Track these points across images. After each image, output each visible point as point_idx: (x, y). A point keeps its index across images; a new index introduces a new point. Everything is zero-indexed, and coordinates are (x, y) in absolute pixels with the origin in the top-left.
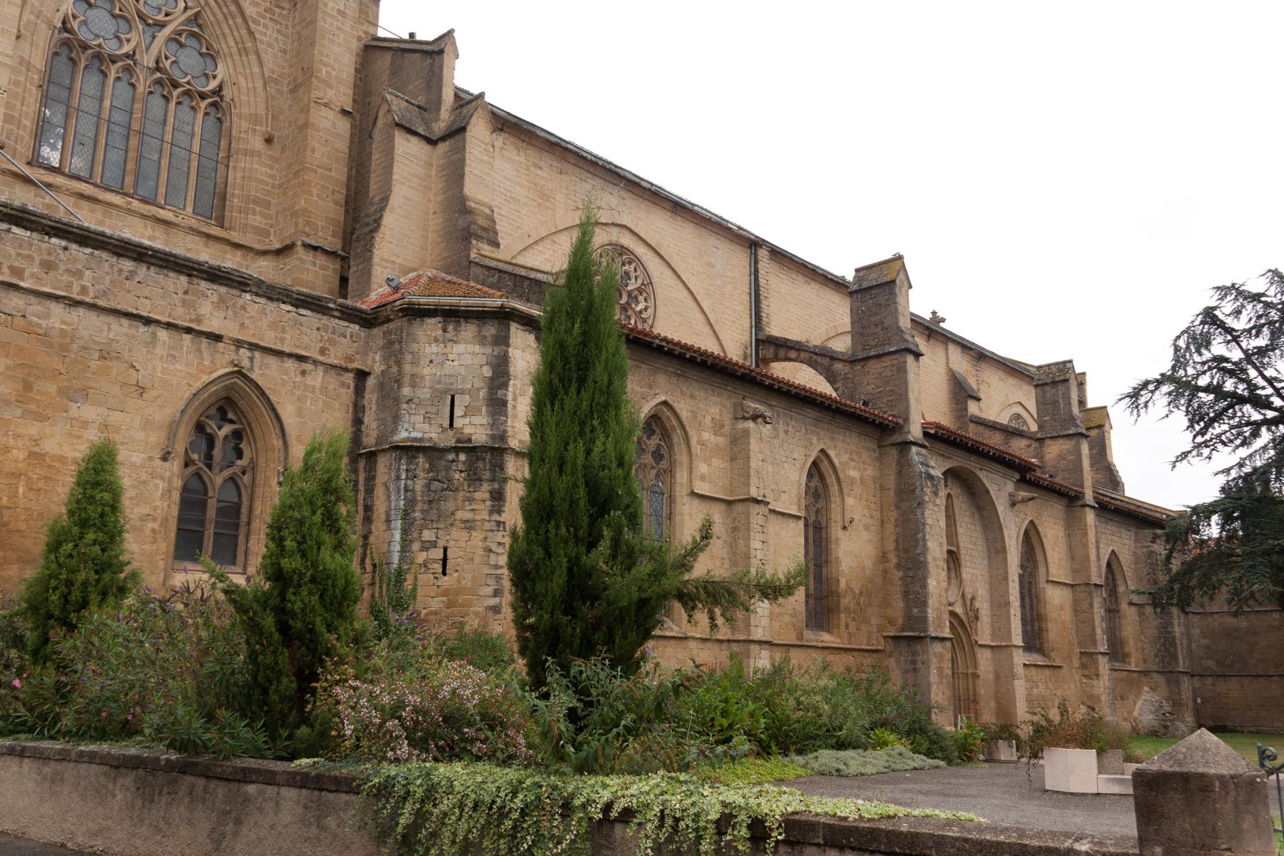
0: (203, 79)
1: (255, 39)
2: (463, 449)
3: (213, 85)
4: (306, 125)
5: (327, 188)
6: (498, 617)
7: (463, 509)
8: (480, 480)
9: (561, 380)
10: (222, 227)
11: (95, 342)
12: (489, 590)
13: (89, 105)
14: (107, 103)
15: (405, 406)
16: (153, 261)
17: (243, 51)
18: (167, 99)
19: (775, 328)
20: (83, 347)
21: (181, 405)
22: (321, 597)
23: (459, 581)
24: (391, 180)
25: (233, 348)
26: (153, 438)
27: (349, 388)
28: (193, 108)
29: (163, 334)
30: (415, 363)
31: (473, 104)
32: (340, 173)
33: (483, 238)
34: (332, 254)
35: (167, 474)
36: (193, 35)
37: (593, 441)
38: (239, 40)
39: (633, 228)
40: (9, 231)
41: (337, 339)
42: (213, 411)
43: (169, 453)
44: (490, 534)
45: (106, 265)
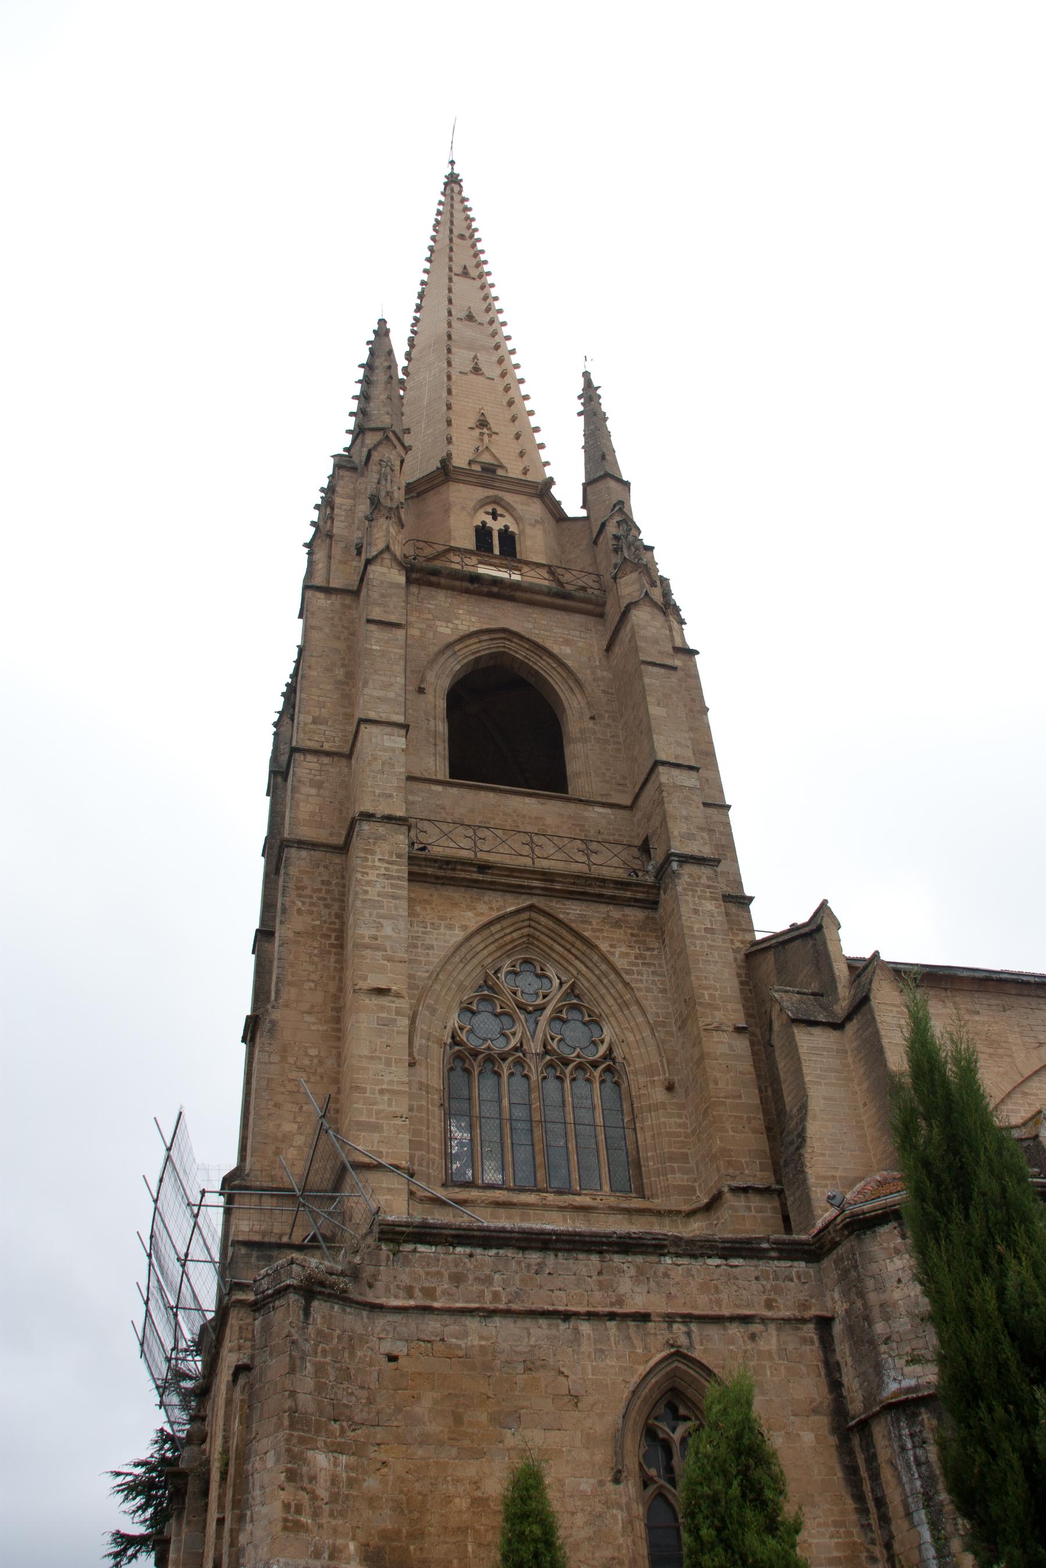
0: (592, 1047)
1: (632, 989)
3: (602, 1049)
4: (702, 1057)
5: (741, 1118)
9: (939, 1206)
10: (644, 1197)
13: (490, 1110)
14: (505, 1102)
15: (883, 1348)
16: (559, 1246)
18: (560, 1079)
20: (506, 1362)
21: (621, 1408)
24: (804, 1083)
25: (665, 1325)
26: (599, 1458)
28: (588, 1080)
29: (585, 1327)
30: (880, 1288)
31: (870, 968)
32: (751, 1097)
34: (764, 1191)
35: (624, 1500)
36: (574, 1007)
37: (1003, 1274)
40: (415, 1251)
41: (783, 1285)
42: (661, 1410)
43: (619, 1472)
45: (514, 1263)
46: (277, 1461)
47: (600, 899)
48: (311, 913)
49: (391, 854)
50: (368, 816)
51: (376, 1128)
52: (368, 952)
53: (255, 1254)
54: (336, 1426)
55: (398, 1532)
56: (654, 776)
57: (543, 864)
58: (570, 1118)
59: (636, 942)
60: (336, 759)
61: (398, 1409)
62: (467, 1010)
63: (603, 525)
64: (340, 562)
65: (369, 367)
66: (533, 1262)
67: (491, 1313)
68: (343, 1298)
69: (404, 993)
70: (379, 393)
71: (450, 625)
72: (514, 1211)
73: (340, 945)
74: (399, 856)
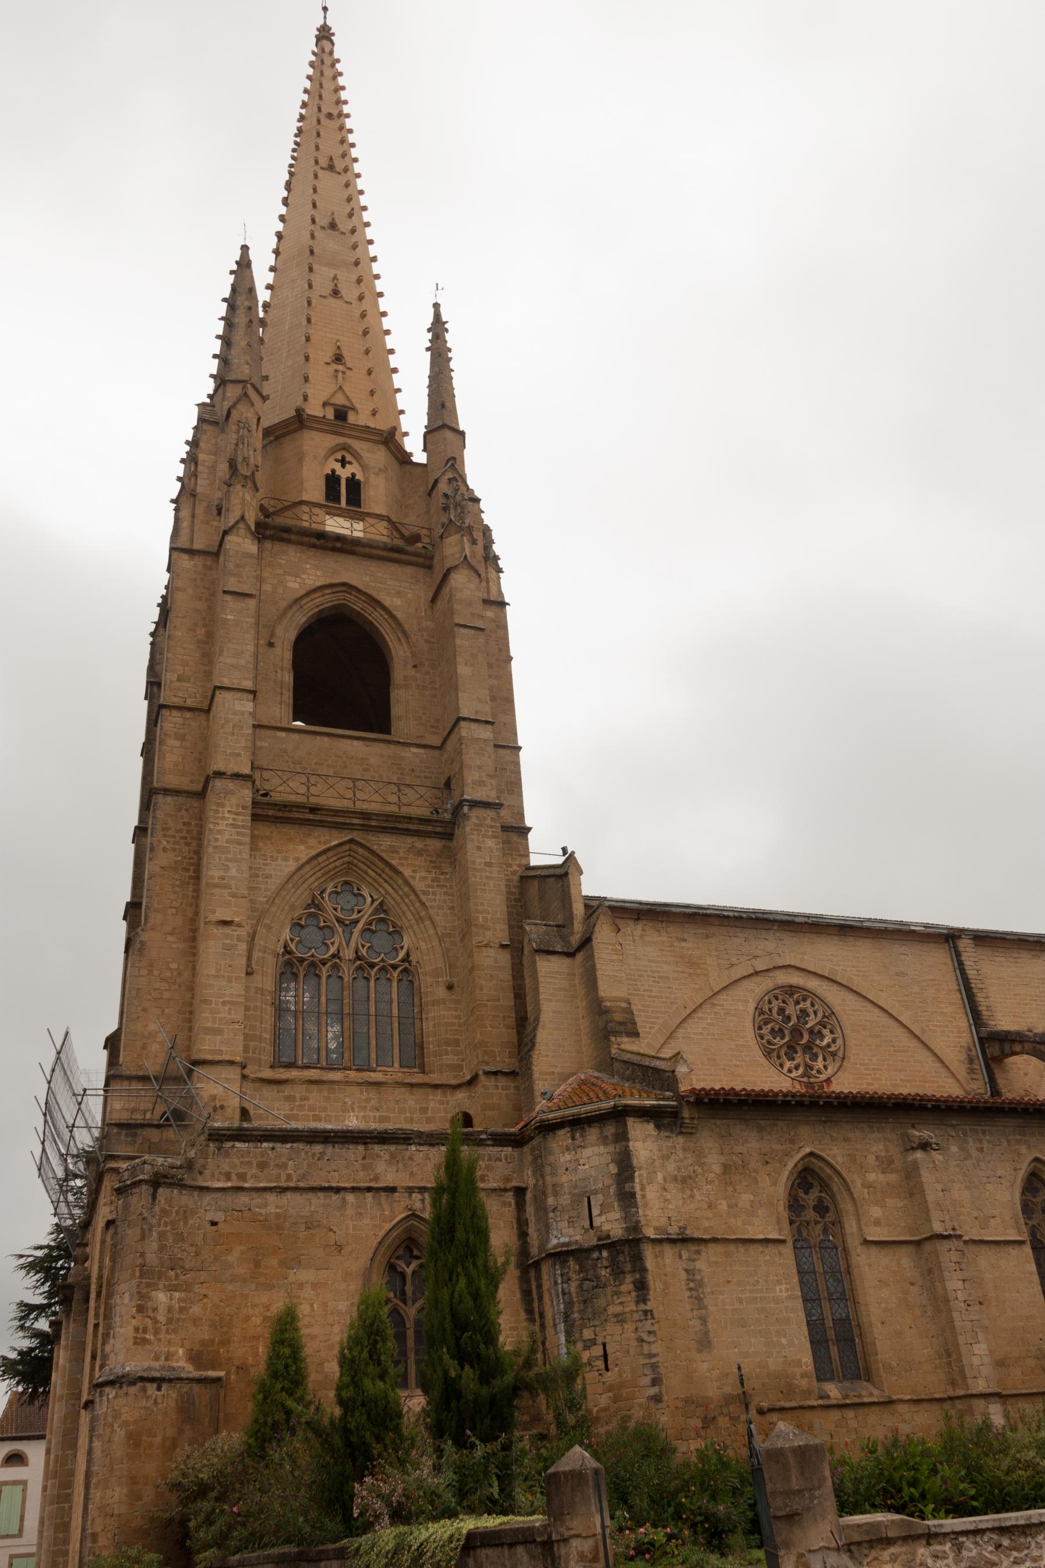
2: (604, 1246)
3: (402, 954)
5: (498, 1017)
6: (660, 1406)
7: (613, 1303)
8: (623, 1272)
11: (302, 1217)
12: (647, 1380)
14: (323, 999)
15: (551, 1215)
16: (336, 1140)
17: (420, 920)
19: (1004, 1022)
22: (369, 1415)
23: (620, 1376)
25: (406, 1195)
26: (352, 1287)
27: (510, 1205)
28: (389, 979)
29: (350, 1197)
30: (554, 1174)
32: (507, 1000)
33: (621, 1033)
38: (414, 912)
39: (798, 965)
40: (233, 1147)
42: (400, 1252)
44: (640, 1324)
45: (303, 1153)
46: (131, 1300)
47: (407, 832)
48: (174, 850)
49: (238, 806)
50: (219, 774)
51: (218, 1032)
52: (217, 890)
53: (124, 1132)
54: (172, 1273)
55: (213, 1341)
56: (456, 730)
57: (360, 806)
58: (373, 1011)
59: (434, 867)
60: (197, 713)
61: (216, 1259)
62: (297, 925)
63: (436, 482)
64: (202, 522)
65: (231, 303)
66: (317, 1151)
67: (284, 1190)
68: (181, 1185)
69: (244, 923)
70: (240, 339)
71: (298, 580)
72: (324, 1087)
73: (197, 877)
74: (244, 808)
